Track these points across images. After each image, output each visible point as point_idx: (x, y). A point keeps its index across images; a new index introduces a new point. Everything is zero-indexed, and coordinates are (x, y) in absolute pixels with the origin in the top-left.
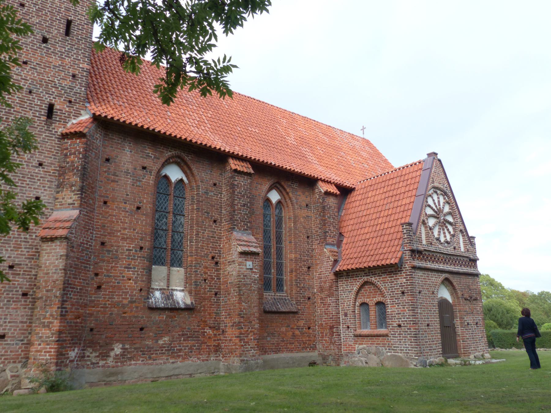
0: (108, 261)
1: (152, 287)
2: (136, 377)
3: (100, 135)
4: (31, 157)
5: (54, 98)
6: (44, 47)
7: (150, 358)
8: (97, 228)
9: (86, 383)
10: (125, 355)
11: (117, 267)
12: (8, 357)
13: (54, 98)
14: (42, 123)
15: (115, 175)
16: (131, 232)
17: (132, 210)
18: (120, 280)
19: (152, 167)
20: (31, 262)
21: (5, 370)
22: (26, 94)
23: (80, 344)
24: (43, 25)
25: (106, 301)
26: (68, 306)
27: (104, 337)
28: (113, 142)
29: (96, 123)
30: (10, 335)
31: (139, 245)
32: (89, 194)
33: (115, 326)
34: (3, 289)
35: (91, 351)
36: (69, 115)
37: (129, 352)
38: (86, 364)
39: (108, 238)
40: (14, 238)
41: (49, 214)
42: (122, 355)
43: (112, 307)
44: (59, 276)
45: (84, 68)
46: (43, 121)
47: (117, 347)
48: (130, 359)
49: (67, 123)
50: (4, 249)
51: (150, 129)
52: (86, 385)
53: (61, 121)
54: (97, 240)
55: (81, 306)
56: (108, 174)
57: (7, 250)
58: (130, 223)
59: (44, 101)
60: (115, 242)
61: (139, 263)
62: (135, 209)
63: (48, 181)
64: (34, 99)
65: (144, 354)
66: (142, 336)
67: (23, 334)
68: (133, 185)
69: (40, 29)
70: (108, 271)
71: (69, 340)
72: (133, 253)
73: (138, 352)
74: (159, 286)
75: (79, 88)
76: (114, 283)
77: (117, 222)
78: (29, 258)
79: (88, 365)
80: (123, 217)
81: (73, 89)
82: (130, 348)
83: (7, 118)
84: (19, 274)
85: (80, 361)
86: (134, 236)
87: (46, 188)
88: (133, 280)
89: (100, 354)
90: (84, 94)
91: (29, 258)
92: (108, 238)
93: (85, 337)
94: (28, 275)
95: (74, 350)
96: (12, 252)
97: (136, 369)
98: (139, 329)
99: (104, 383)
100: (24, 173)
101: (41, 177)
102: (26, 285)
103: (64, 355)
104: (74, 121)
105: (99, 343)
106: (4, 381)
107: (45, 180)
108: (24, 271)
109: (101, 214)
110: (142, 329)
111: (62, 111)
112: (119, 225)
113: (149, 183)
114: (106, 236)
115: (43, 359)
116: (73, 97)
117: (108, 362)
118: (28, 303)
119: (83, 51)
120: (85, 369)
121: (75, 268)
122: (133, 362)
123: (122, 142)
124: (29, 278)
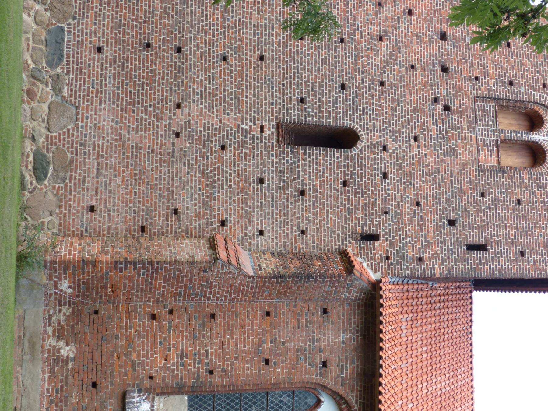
0: (189, 326)
1: (156, 398)
2: (25, 381)
3: (356, 298)
4: (310, 221)
6: (444, 222)
7: (51, 402)
8: (233, 306)
9: (25, 311)
11: (183, 340)
13: (387, 238)
14: (352, 228)
15: (308, 323)
17: (263, 352)
18: (165, 346)
19: (328, 376)
20: (183, 232)
21: (51, 215)
22: (382, 208)
23: (78, 296)
25: (135, 328)
26: (129, 272)
27: (86, 329)
28: (351, 316)
29: (369, 288)
31: (215, 368)
32: (276, 287)
33: (100, 344)
34: (149, 205)
35: (68, 314)
36: (371, 259)
37: (62, 368)
38: (50, 309)
39: (221, 322)
41: (244, 246)
43: (126, 337)
44: (166, 255)
45: (434, 270)
46: (356, 230)
47: (71, 350)
48: (52, 372)
49: (361, 257)
50: (197, 202)
51: (381, 362)
52: (21, 311)
53: (360, 250)
56: (306, 314)
57: (195, 205)
58: (245, 352)
59: (380, 229)
60: (216, 333)
61: (189, 372)
62: (265, 356)
64: (380, 218)
65: (57, 392)
66: (85, 386)
67: (95, 231)
68: (298, 350)
69: (462, 216)
70: (177, 326)
71: (83, 278)
72: (203, 360)
73: (62, 381)
75: (407, 266)
77: (244, 334)
78: (187, 229)
79: (49, 312)
80: (252, 340)
81: (404, 260)
82: (68, 370)
83: (349, 191)
84: (167, 220)
85: (55, 299)
87: (275, 241)
88: (165, 364)
89: (63, 327)
90: (402, 273)
91: (187, 229)
92: (221, 322)
93: (87, 304)
94: (167, 230)
95: (70, 287)
96: (193, 211)
98: (94, 380)
99: (22, 334)
100: (290, 215)
101: (288, 234)
102: (155, 229)
103: (65, 273)
104: (365, 264)
106: (38, 215)
107: (284, 238)
109: (252, 309)
110: (94, 385)
111: (374, 250)
112: (240, 336)
113: (305, 374)
114: (224, 318)
115: (61, 248)
116: (394, 261)
117: (51, 339)
118: (132, 233)
119: (455, 267)
120: (43, 308)
121: (178, 277)
122: (47, 376)
123: (354, 328)
124: (163, 232)
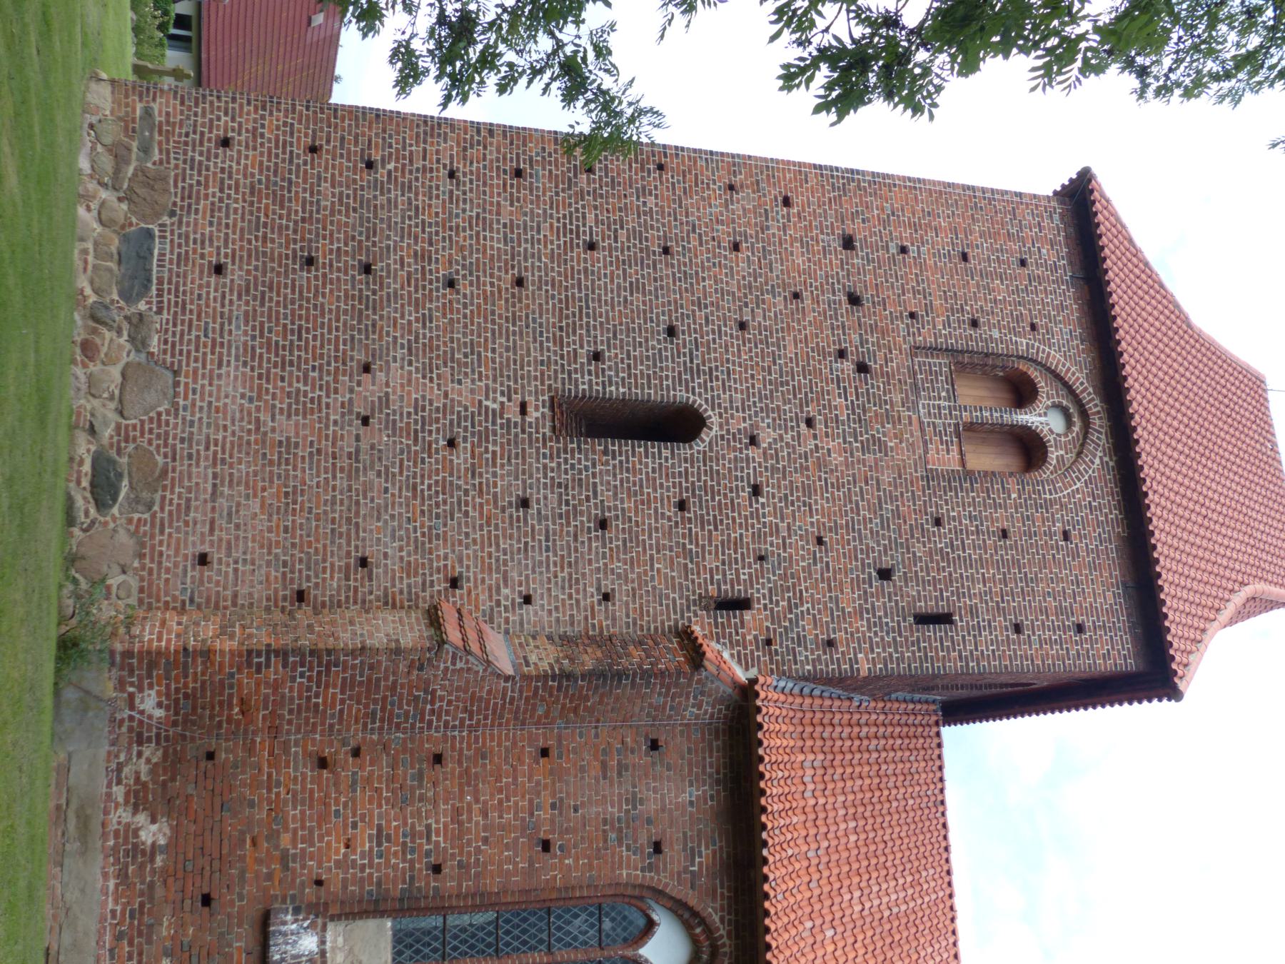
0: (392, 779)
1: (330, 926)
2: (68, 895)
4: (619, 576)
5: (765, 605)
6: (870, 574)
8: (477, 738)
9: (70, 755)
10: (134, 857)
11: (380, 806)
12: (155, 576)
13: (765, 605)
15: (622, 768)
16: (477, 833)
17: (537, 827)
18: (345, 819)
21: (124, 572)
22: (754, 550)
24: (915, 565)
25: (286, 786)
26: (274, 672)
27: (190, 789)
28: (703, 752)
29: (736, 697)
30: (206, 574)
31: (445, 861)
34: (312, 551)
35: (155, 760)
37: (142, 866)
38: (119, 751)
39: (453, 770)
40: (431, 560)
42: (135, 846)
43: (269, 803)
44: (346, 638)
45: (857, 663)
46: (707, 590)
47: (160, 830)
48: (122, 875)
49: (718, 642)
50: (404, 543)
51: (764, 835)
52: (63, 755)
54: (446, 742)
55: (273, 713)
57: (401, 549)
58: (502, 827)
59: (752, 587)
60: (445, 790)
61: (394, 869)
62: (542, 835)
63: (572, 616)
64: (750, 567)
65: (132, 917)
66: (188, 902)
68: (605, 822)
70: (369, 780)
72: (421, 845)
73: (142, 894)
74: (333, 949)
75: (806, 657)
76: (337, 800)
77: (500, 792)
78: (386, 595)
79: (117, 756)
80: (516, 803)
81: (799, 645)
82: (153, 871)
83: (690, 519)
84: (348, 579)
85: (131, 729)
86: (469, 842)
87: (554, 614)
88: (345, 855)
89: (145, 785)
91: (386, 595)
92: (453, 770)
94: (347, 597)
95: (160, 705)
96: (397, 560)
97: (92, 891)
98: (206, 890)
99: (63, 801)
100: (580, 565)
101: (578, 601)
102: (324, 595)
103: (150, 676)
105: (173, 779)
107: (572, 609)
108: (356, 589)
109: (514, 744)
111: (743, 627)
112: (492, 795)
113: (620, 868)
114: (460, 763)
117: (120, 810)
119: (895, 655)
120: (107, 748)
121: (369, 680)
122: (112, 884)
123: (711, 776)
124: (339, 601)
